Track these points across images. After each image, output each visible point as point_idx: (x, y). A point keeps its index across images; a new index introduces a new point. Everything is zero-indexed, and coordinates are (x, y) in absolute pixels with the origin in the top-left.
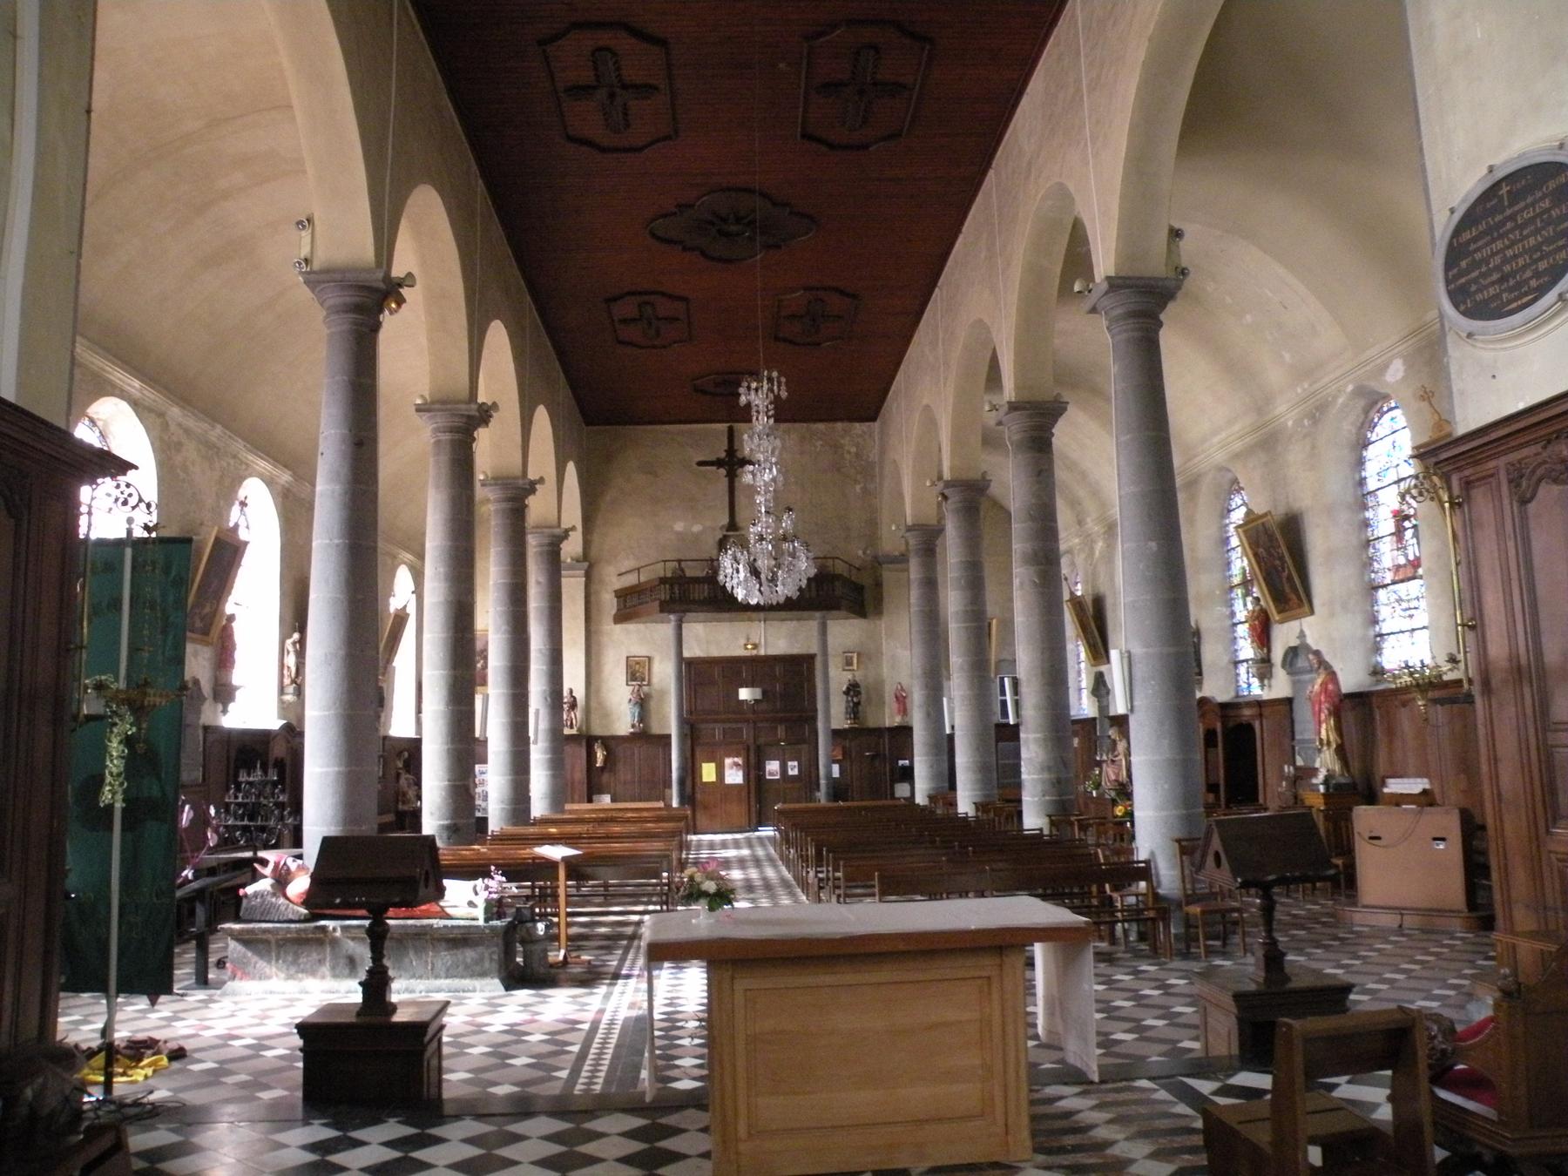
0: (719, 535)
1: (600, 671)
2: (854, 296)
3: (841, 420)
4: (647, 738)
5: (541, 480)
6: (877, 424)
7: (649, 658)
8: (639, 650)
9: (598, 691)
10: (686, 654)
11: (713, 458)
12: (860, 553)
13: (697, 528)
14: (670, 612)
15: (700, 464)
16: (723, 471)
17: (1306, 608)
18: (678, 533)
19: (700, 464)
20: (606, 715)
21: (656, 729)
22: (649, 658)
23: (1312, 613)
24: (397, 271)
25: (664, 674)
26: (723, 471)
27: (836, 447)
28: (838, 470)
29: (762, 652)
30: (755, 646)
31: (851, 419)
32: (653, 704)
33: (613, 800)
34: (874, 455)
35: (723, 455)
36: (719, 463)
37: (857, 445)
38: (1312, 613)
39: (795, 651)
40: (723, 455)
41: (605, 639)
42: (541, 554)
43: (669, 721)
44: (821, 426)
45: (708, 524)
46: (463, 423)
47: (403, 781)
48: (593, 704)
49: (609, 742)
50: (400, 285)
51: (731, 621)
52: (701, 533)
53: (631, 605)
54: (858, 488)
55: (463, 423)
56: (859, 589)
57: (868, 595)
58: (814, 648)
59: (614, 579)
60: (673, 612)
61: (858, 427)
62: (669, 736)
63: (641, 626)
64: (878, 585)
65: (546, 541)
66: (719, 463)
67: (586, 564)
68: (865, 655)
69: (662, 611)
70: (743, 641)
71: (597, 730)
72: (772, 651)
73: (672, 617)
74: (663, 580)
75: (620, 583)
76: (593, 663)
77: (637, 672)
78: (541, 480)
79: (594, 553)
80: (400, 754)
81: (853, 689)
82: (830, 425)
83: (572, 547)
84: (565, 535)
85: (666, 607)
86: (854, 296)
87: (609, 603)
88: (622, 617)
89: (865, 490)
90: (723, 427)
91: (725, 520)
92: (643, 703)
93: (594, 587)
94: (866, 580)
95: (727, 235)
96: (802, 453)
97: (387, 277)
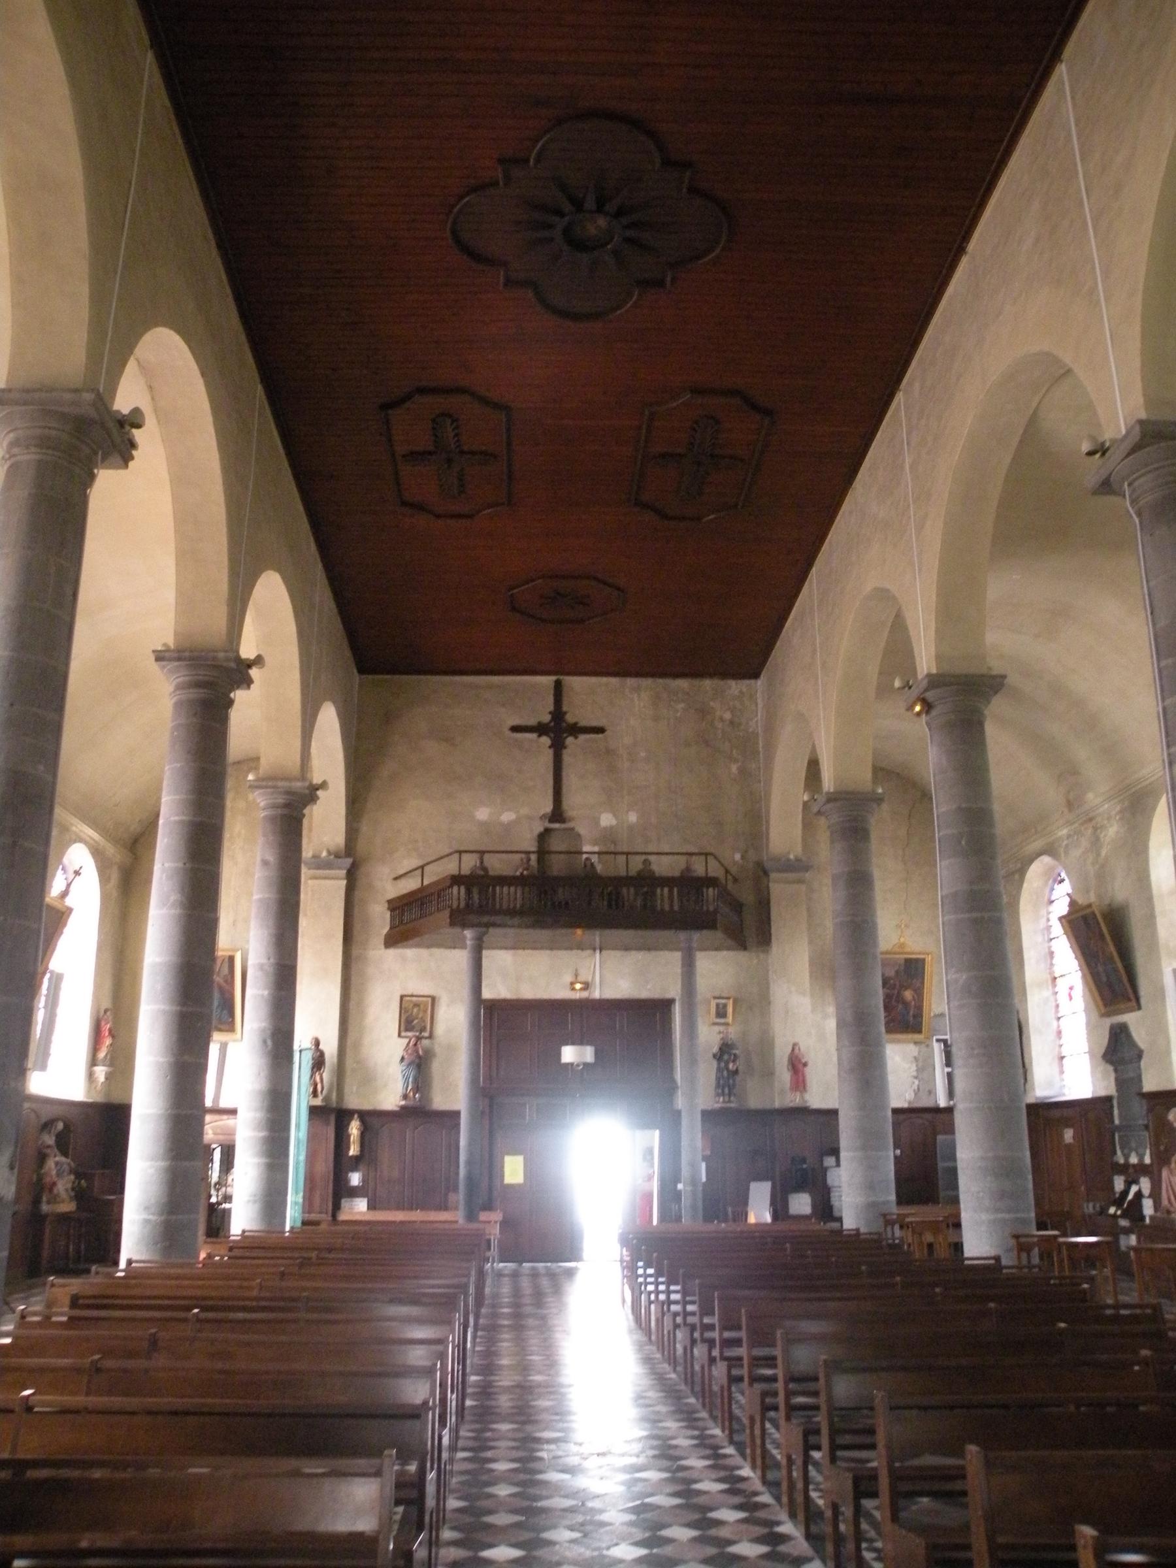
0: (539, 828)
1: (362, 1013)
2: (768, 412)
3: (711, 676)
4: (418, 1113)
5: (324, 785)
6: (760, 684)
7: (433, 999)
8: (419, 987)
9: (357, 1046)
10: (487, 994)
11: (532, 722)
12: (738, 857)
13: (507, 817)
14: (464, 925)
15: (515, 729)
16: (546, 740)
17: (1134, 1003)
18: (482, 824)
19: (515, 729)
20: (368, 1079)
21: (440, 1102)
22: (433, 999)
23: (1139, 1008)
24: (247, 651)
25: (453, 1021)
26: (546, 740)
27: (704, 712)
28: (707, 743)
29: (596, 995)
30: (587, 986)
31: (725, 675)
32: (436, 1066)
33: (371, 1207)
34: (757, 724)
35: (546, 718)
36: (540, 729)
37: (733, 710)
38: (1139, 1008)
39: (644, 994)
40: (546, 718)
41: (371, 970)
42: (272, 819)
43: (453, 1090)
44: (683, 684)
45: (525, 811)
46: (212, 680)
47: (50, 1164)
48: (349, 1063)
49: (371, 1119)
50: (249, 667)
51: (552, 946)
52: (517, 821)
53: (411, 920)
54: (734, 768)
55: (212, 680)
56: (738, 907)
57: (749, 919)
58: (674, 990)
59: (389, 882)
60: (472, 926)
61: (735, 687)
62: (457, 1114)
63: (424, 952)
64: (764, 905)
65: (281, 800)
66: (540, 729)
67: (348, 861)
68: (753, 1001)
69: (452, 924)
70: (568, 978)
71: (353, 1101)
72: (611, 993)
73: (468, 934)
74: (456, 880)
75: (394, 890)
76: (352, 1005)
77: (415, 1018)
78: (324, 785)
79: (361, 846)
80: (47, 1126)
81: (725, 1051)
82: (696, 682)
83: (326, 824)
84: (310, 795)
85: (459, 918)
86: (768, 412)
87: (379, 918)
88: (396, 938)
89: (743, 771)
90: (548, 681)
91: (548, 808)
92: (420, 1064)
93: (358, 894)
94: (747, 897)
95: (579, 245)
96: (656, 719)
97: (238, 660)
